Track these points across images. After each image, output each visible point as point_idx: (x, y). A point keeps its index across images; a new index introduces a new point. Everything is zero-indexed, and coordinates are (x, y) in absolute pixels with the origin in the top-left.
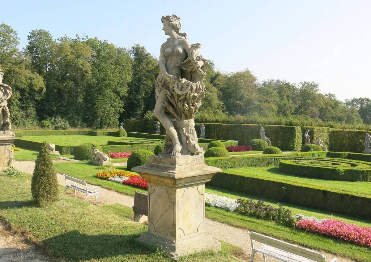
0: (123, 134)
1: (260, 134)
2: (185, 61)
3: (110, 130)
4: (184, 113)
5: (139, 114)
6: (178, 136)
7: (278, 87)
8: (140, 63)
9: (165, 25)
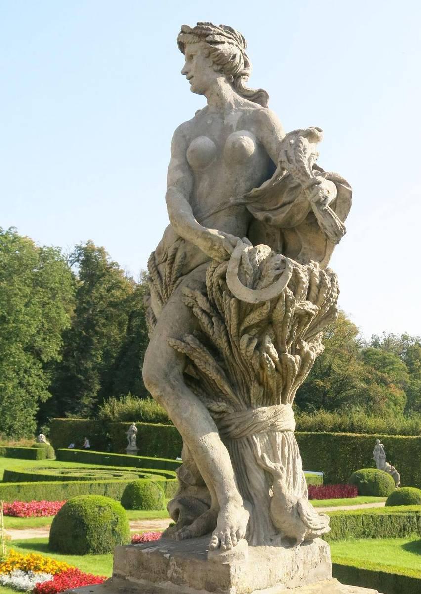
0: (44, 454)
1: (373, 456)
2: (265, 184)
3: (12, 444)
4: (257, 377)
5: (86, 406)
6: (234, 469)
7: (405, 351)
8: (92, 284)
9: (190, 58)
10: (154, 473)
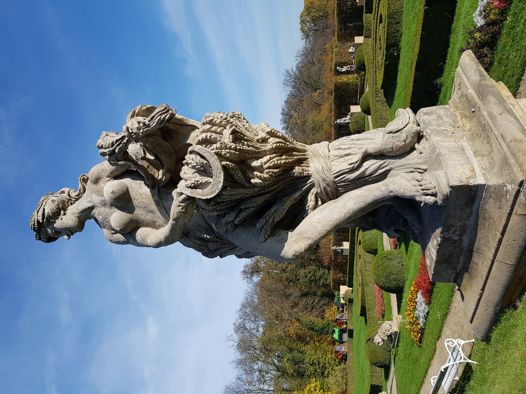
10: (358, 237)
